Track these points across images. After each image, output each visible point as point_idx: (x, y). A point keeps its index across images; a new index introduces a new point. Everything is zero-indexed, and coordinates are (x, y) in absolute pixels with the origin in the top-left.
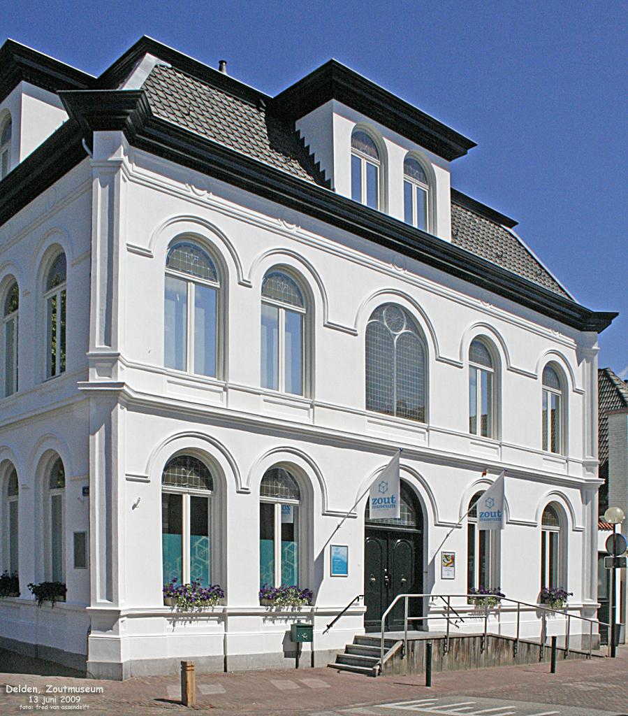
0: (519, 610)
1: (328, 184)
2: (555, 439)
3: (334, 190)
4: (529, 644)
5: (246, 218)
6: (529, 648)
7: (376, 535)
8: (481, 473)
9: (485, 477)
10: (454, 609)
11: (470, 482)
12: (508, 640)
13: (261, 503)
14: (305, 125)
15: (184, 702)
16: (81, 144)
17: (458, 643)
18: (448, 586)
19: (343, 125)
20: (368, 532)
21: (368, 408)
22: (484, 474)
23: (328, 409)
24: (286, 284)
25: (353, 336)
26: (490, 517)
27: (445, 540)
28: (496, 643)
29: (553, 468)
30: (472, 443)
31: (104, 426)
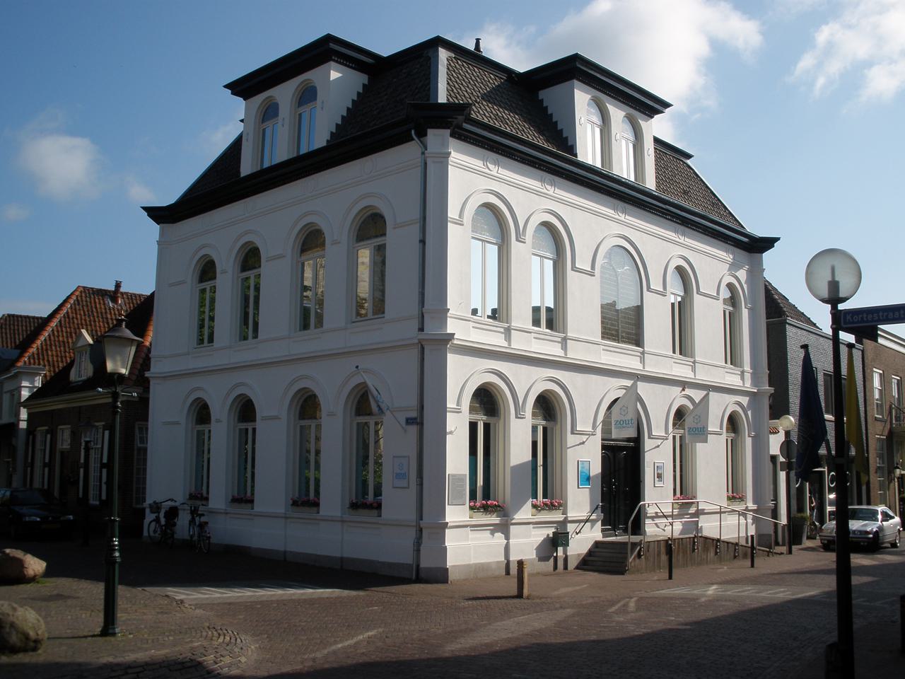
0: (721, 513)
1: (571, 149)
2: (733, 357)
3: (576, 155)
4: (728, 543)
5: (524, 187)
6: (728, 546)
7: (610, 451)
8: (681, 389)
9: (683, 393)
10: (665, 514)
11: (614, 388)
12: (713, 540)
13: (533, 427)
14: (549, 96)
15: (520, 595)
16: (411, 135)
17: (679, 543)
18: (657, 496)
19: (582, 98)
20: (604, 447)
21: (603, 338)
22: (683, 390)
23: (869, 427)
24: (555, 238)
25: (589, 277)
26: (624, 425)
27: (658, 455)
28: (705, 544)
29: (681, 370)
30: (674, 362)
31: (638, 404)
